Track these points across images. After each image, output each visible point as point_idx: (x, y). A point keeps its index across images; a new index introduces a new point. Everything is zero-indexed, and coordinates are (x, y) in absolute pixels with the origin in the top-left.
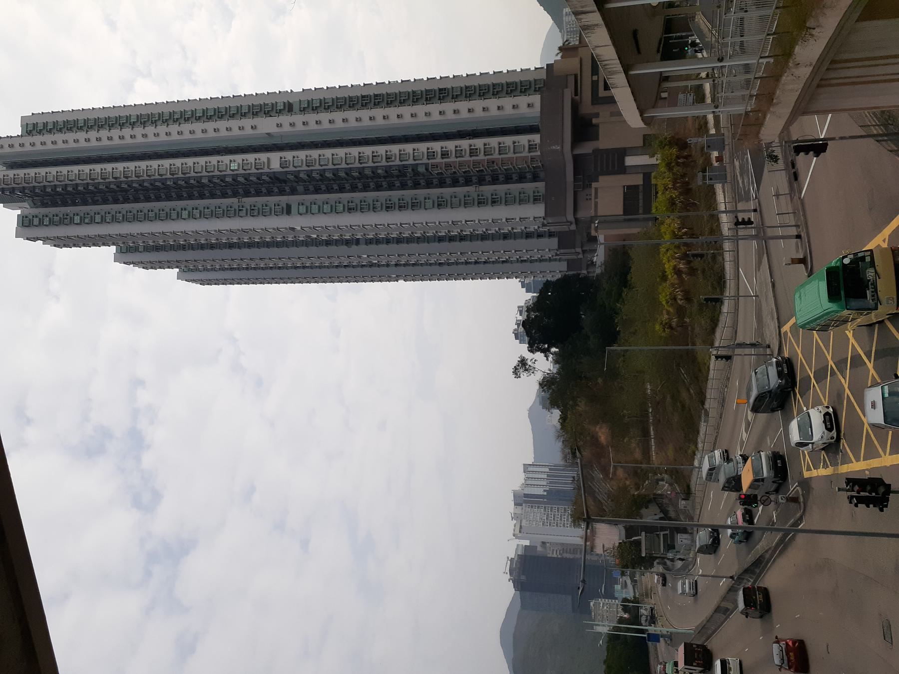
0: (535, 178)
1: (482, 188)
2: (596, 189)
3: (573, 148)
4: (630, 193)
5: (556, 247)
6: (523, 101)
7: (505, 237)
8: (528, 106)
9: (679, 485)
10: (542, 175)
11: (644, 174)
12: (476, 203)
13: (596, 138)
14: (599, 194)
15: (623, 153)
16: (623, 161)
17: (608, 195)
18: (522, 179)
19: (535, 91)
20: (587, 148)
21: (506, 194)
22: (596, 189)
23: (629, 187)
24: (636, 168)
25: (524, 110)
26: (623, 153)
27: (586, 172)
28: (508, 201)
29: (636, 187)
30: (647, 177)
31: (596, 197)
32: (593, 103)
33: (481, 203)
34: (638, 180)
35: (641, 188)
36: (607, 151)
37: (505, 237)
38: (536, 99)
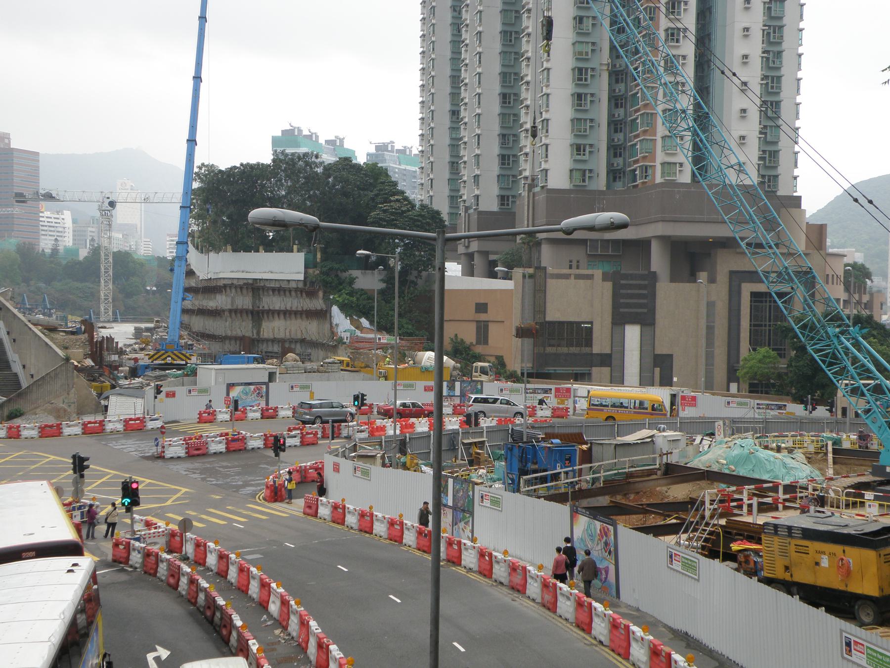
0: (614, 174)
1: (605, 76)
2: (590, 277)
3: (663, 239)
4: (580, 334)
5: (482, 208)
6: (751, 155)
7: (455, 113)
8: (740, 161)
9: (367, 318)
10: (619, 186)
11: (609, 356)
12: (581, 65)
13: (675, 278)
14: (581, 282)
15: (647, 320)
16: (633, 322)
17: (582, 297)
18: (615, 150)
19: (763, 176)
20: (658, 261)
21: (592, 120)
22: (590, 277)
23: (590, 331)
24: (619, 342)
25: (737, 155)
26: (647, 320)
27: (621, 255)
28: (581, 125)
29: (589, 342)
30: (605, 360)
31: (578, 277)
32: (732, 273)
33: (581, 74)
34: (601, 345)
35: (585, 350)
36: (653, 296)
37: (455, 113)
38: (752, 178)
